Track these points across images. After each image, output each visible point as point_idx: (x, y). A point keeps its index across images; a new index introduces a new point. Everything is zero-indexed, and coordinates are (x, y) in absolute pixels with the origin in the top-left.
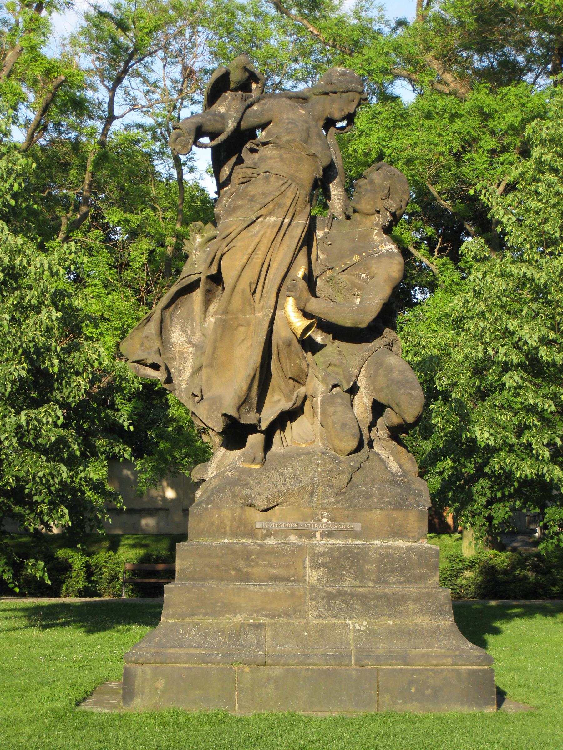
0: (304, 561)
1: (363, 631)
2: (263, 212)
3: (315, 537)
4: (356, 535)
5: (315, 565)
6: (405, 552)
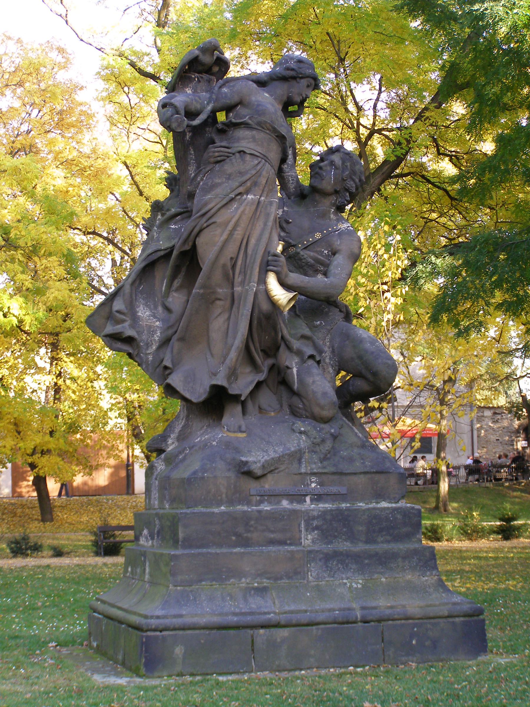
0: (299, 525)
1: (360, 589)
2: (241, 190)
3: (305, 502)
4: (342, 497)
5: (310, 528)
6: (391, 513)
